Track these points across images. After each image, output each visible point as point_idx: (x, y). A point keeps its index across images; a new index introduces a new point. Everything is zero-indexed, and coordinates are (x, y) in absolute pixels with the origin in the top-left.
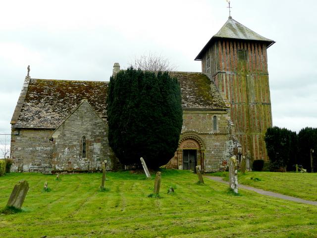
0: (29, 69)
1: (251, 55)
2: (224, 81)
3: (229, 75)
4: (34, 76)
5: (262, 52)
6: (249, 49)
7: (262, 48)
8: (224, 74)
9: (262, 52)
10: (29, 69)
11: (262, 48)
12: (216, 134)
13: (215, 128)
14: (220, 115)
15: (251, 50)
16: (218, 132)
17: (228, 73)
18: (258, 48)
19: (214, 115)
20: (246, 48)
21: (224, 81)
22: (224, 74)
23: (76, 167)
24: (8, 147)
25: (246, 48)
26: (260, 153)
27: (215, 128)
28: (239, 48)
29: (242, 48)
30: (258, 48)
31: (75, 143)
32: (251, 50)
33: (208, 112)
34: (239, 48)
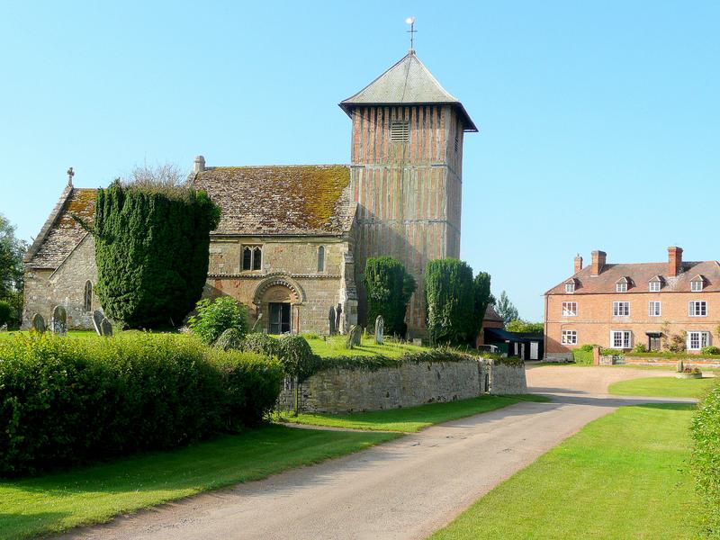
0: (71, 173)
1: (75, 200)
2: (360, 181)
3: (371, 170)
4: (78, 184)
5: (439, 122)
6: (414, 118)
7: (439, 115)
8: (361, 170)
9: (439, 122)
10: (71, 173)
11: (439, 115)
12: (321, 278)
13: (320, 268)
14: (330, 246)
15: (418, 121)
16: (325, 273)
17: (368, 166)
18: (432, 113)
19: (321, 245)
20: (407, 117)
21: (360, 181)
22: (361, 170)
23: (78, 324)
24: (347, 249)
25: (407, 117)
26: (415, 312)
27: (320, 268)
28: (394, 118)
29: (400, 117)
30: (432, 113)
31: (78, 291)
32: (418, 121)
33: (309, 240)
34: (394, 118)
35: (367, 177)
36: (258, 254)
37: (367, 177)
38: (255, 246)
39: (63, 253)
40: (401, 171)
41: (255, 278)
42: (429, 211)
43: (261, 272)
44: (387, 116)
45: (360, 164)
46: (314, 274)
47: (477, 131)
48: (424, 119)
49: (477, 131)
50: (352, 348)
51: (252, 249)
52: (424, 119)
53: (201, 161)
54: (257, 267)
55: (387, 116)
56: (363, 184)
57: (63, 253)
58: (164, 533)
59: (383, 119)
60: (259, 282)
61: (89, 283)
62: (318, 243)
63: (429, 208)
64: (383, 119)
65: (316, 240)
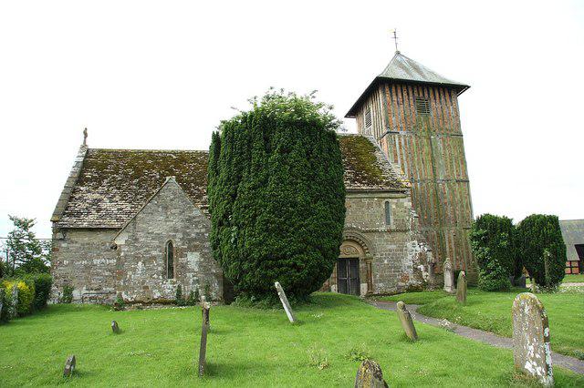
12: (390, 231)
14: (395, 201)
16: (393, 227)
19: (386, 200)
23: (157, 295)
25: (426, 95)
35: (403, 143)
37: (403, 143)
39: (98, 211)
44: (411, 92)
45: (395, 130)
46: (383, 228)
47: (469, 87)
48: (440, 98)
49: (469, 87)
50: (414, 337)
52: (440, 98)
55: (411, 92)
57: (98, 211)
59: (408, 94)
61: (170, 244)
62: (385, 198)
65: (383, 195)
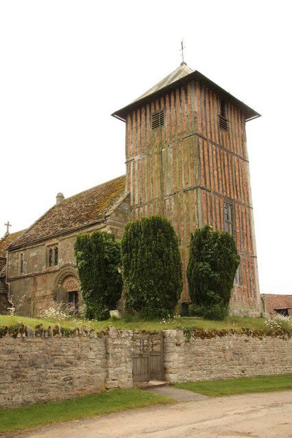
6: (167, 104)
10: (8, 225)
11: (186, 93)
20: (162, 105)
29: (158, 107)
34: (153, 111)
35: (136, 168)
36: (56, 250)
38: (54, 245)
40: (161, 153)
41: (54, 272)
42: (183, 182)
43: (57, 267)
47: (259, 116)
48: (175, 101)
49: (259, 116)
51: (53, 248)
53: (60, 197)
54: (56, 263)
56: (134, 174)
58: (49, 434)
59: (146, 115)
60: (57, 274)
63: (183, 179)
64: (146, 115)
